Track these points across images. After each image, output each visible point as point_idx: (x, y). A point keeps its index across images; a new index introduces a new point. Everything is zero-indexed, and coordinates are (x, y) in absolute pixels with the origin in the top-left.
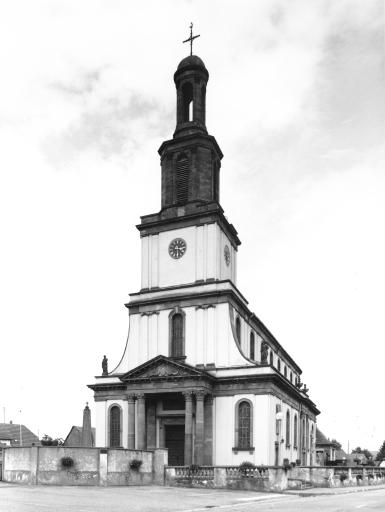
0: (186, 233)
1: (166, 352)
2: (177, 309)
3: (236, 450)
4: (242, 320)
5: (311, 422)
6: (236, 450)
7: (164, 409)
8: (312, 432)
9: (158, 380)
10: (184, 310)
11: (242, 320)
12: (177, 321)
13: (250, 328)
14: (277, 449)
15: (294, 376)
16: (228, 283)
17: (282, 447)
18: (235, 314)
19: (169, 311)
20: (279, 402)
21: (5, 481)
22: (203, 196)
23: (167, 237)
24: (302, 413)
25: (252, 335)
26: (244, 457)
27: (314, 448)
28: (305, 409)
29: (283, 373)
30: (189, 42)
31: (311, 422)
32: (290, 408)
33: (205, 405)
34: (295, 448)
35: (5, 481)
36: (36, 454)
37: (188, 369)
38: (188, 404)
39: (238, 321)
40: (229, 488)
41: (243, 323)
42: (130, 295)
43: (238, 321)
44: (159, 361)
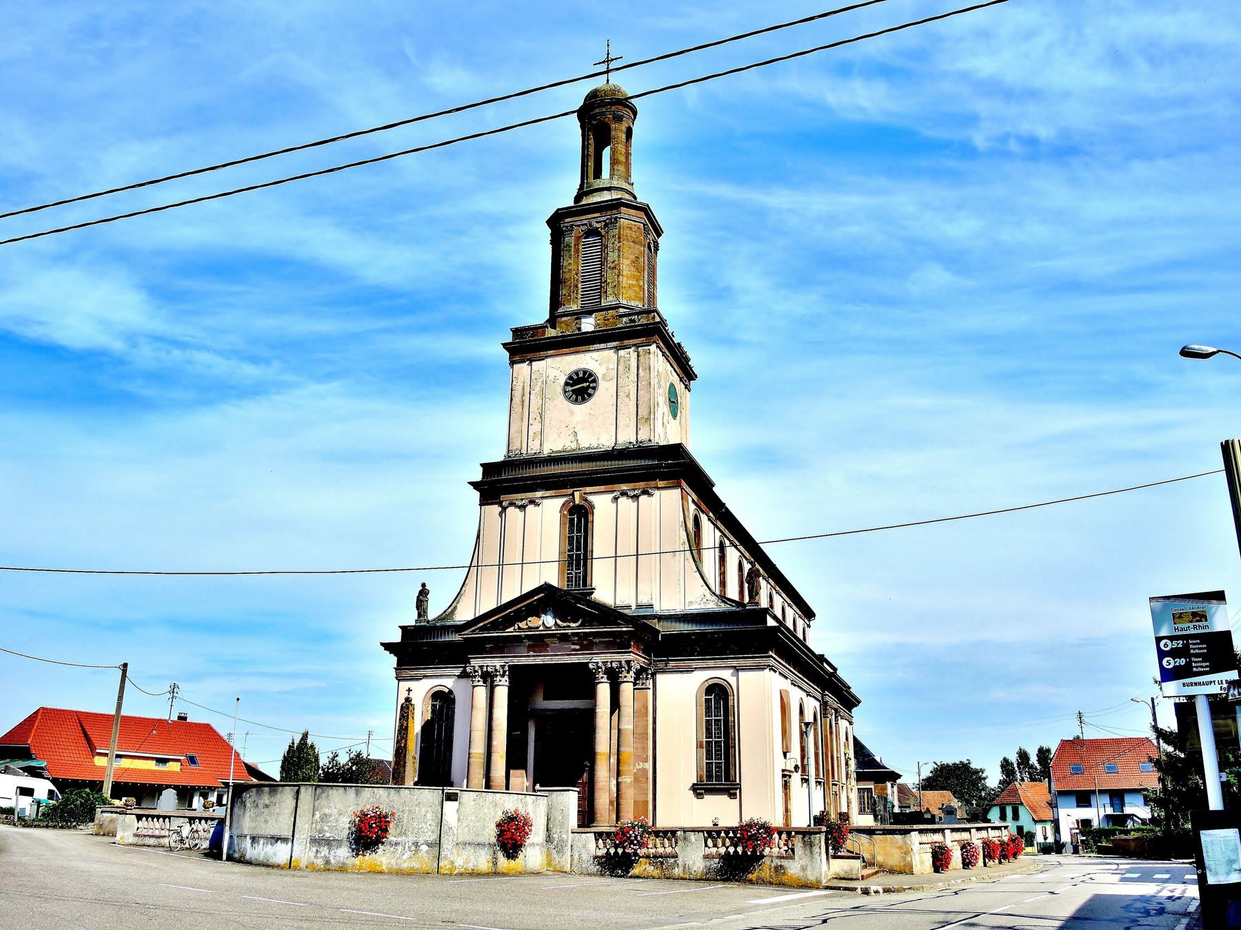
0: (597, 361)
3: (699, 790)
4: (704, 518)
5: (843, 724)
6: (699, 790)
10: (590, 498)
11: (704, 518)
12: (579, 519)
14: (786, 786)
15: (800, 623)
18: (692, 507)
21: (176, 788)
23: (559, 367)
24: (824, 705)
25: (722, 548)
26: (872, 892)
28: (831, 700)
30: (611, 56)
32: (804, 695)
33: (453, 612)
34: (818, 783)
36: (291, 803)
37: (609, 615)
40: (707, 878)
42: (1151, 599)
44: (545, 599)
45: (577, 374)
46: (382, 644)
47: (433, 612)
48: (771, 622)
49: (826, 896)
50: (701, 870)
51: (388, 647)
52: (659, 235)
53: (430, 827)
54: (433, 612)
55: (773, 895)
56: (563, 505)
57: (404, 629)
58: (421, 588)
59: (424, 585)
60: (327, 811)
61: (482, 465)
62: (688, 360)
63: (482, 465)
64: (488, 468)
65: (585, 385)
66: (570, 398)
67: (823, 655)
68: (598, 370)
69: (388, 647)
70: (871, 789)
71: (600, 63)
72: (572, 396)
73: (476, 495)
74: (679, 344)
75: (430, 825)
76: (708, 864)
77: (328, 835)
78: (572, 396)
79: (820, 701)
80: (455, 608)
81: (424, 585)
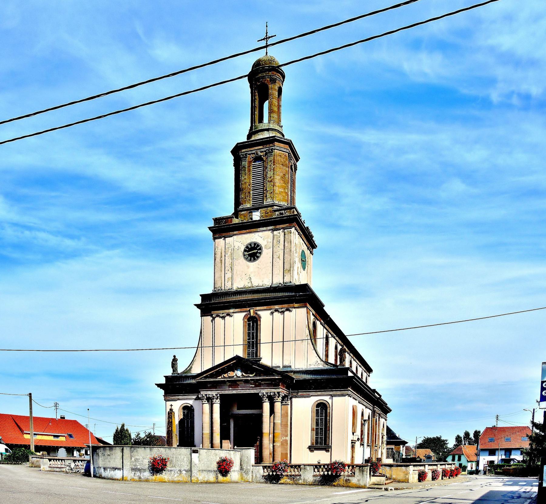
1: (240, 352)
2: (252, 311)
3: (312, 448)
4: (318, 323)
5: (382, 420)
6: (312, 448)
7: (239, 409)
8: (383, 430)
9: (234, 383)
10: (259, 313)
11: (318, 323)
13: (285, 137)
15: (365, 375)
16: (287, 147)
17: (358, 444)
18: (312, 317)
19: (244, 314)
20: (356, 403)
22: (281, 201)
25: (327, 338)
26: (322, 457)
27: (385, 445)
28: (377, 410)
29: (360, 376)
31: (382, 420)
35: (65, 447)
38: (266, 406)
39: (314, 324)
41: (320, 328)
43: (314, 324)
52: (297, 160)
53: (186, 464)
57: (166, 377)
59: (174, 356)
60: (137, 457)
65: (255, 251)
69: (159, 386)
74: (307, 227)
80: (191, 367)
81: (174, 356)
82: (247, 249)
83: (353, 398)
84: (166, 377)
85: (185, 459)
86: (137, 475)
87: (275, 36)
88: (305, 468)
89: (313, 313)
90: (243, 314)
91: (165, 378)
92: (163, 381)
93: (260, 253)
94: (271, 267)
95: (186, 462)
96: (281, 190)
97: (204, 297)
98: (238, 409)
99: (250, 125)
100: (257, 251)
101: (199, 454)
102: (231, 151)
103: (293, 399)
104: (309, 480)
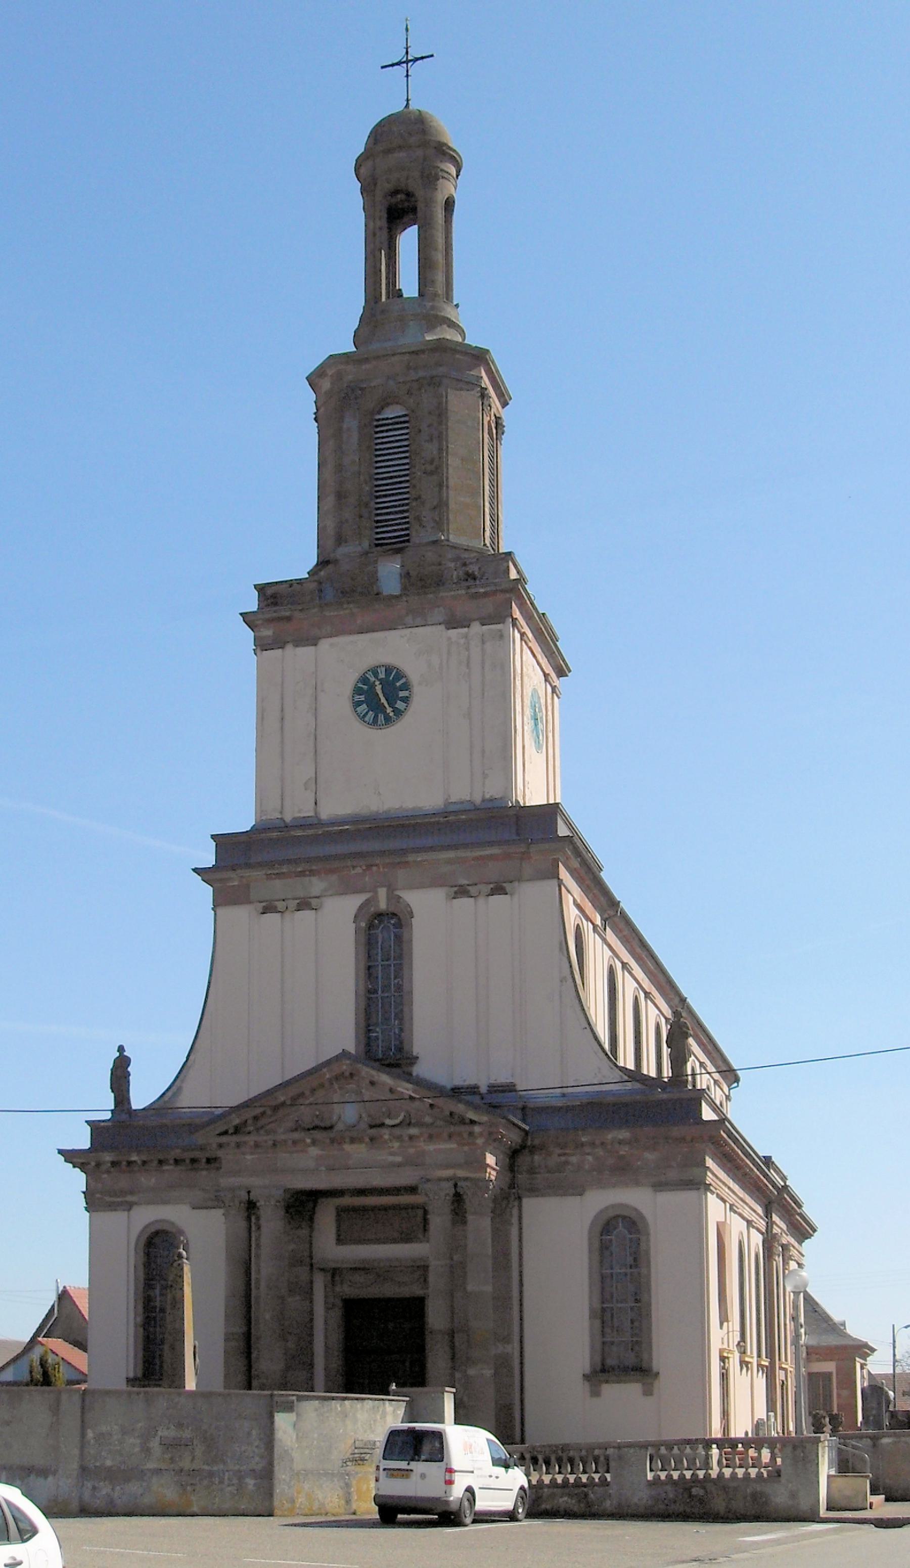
45: (406, 700)
46: (61, 1152)
47: (141, 1097)
48: (708, 1114)
49: (834, 1529)
50: (645, 1501)
51: (70, 1156)
52: (505, 404)
53: (256, 1450)
54: (141, 1097)
55: (771, 1532)
56: (361, 908)
57: (94, 1126)
58: (118, 1054)
59: (121, 1049)
60: (104, 1429)
61: (213, 837)
62: (555, 639)
63: (213, 837)
64: (223, 842)
65: (378, 688)
66: (364, 716)
67: (770, 1157)
68: (413, 669)
69: (70, 1156)
70: (830, 1374)
71: (392, 65)
72: (367, 713)
73: (207, 892)
74: (543, 614)
75: (257, 1447)
76: (653, 1493)
77: (109, 1463)
78: (367, 713)
79: (762, 1233)
80: (180, 1089)
81: (121, 1049)
82: (365, 687)
83: (718, 1195)
84: (94, 1126)
85: (254, 1432)
86: (104, 1492)
87: (432, 56)
88: (620, 1458)
89: (575, 900)
90: (353, 903)
91: (89, 1128)
92: (84, 1142)
93: (375, 673)
94: (643, 980)
95: (256, 1444)
96: (462, 499)
97: (223, 842)
98: (340, 1241)
99: (362, 303)
100: (377, 683)
101: (297, 1414)
102: (307, 375)
103: (525, 1201)
104: (636, 1500)
